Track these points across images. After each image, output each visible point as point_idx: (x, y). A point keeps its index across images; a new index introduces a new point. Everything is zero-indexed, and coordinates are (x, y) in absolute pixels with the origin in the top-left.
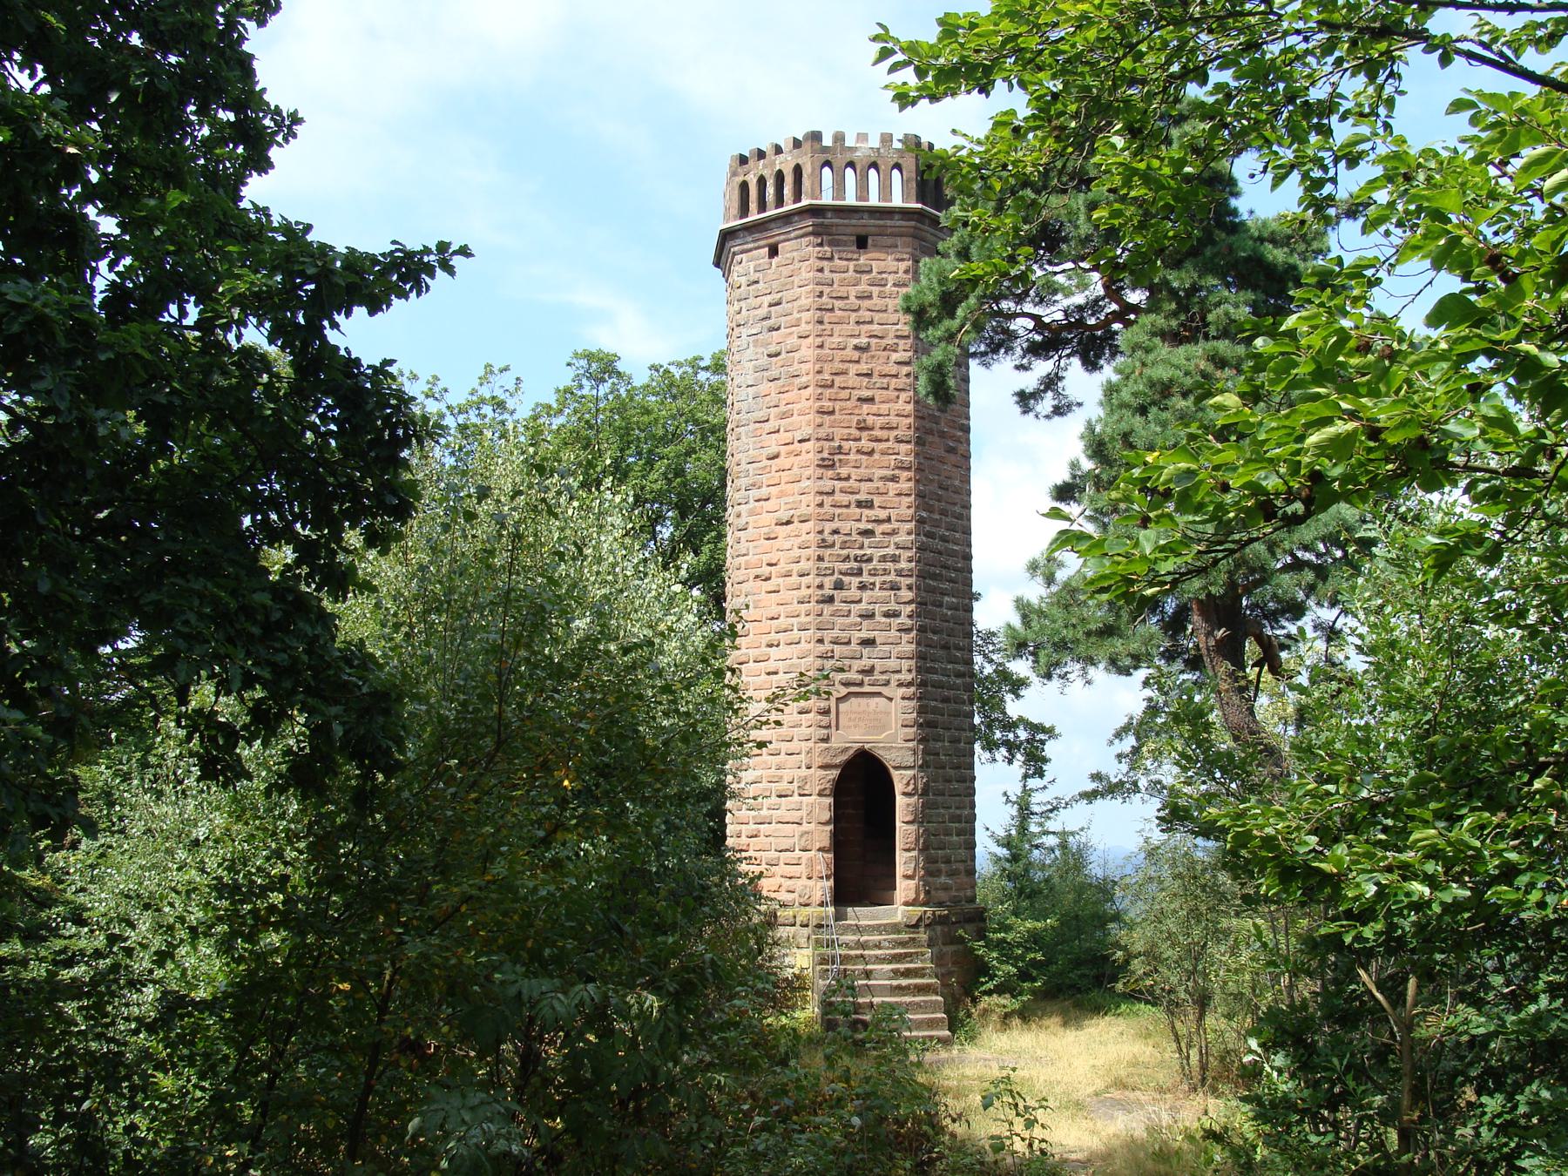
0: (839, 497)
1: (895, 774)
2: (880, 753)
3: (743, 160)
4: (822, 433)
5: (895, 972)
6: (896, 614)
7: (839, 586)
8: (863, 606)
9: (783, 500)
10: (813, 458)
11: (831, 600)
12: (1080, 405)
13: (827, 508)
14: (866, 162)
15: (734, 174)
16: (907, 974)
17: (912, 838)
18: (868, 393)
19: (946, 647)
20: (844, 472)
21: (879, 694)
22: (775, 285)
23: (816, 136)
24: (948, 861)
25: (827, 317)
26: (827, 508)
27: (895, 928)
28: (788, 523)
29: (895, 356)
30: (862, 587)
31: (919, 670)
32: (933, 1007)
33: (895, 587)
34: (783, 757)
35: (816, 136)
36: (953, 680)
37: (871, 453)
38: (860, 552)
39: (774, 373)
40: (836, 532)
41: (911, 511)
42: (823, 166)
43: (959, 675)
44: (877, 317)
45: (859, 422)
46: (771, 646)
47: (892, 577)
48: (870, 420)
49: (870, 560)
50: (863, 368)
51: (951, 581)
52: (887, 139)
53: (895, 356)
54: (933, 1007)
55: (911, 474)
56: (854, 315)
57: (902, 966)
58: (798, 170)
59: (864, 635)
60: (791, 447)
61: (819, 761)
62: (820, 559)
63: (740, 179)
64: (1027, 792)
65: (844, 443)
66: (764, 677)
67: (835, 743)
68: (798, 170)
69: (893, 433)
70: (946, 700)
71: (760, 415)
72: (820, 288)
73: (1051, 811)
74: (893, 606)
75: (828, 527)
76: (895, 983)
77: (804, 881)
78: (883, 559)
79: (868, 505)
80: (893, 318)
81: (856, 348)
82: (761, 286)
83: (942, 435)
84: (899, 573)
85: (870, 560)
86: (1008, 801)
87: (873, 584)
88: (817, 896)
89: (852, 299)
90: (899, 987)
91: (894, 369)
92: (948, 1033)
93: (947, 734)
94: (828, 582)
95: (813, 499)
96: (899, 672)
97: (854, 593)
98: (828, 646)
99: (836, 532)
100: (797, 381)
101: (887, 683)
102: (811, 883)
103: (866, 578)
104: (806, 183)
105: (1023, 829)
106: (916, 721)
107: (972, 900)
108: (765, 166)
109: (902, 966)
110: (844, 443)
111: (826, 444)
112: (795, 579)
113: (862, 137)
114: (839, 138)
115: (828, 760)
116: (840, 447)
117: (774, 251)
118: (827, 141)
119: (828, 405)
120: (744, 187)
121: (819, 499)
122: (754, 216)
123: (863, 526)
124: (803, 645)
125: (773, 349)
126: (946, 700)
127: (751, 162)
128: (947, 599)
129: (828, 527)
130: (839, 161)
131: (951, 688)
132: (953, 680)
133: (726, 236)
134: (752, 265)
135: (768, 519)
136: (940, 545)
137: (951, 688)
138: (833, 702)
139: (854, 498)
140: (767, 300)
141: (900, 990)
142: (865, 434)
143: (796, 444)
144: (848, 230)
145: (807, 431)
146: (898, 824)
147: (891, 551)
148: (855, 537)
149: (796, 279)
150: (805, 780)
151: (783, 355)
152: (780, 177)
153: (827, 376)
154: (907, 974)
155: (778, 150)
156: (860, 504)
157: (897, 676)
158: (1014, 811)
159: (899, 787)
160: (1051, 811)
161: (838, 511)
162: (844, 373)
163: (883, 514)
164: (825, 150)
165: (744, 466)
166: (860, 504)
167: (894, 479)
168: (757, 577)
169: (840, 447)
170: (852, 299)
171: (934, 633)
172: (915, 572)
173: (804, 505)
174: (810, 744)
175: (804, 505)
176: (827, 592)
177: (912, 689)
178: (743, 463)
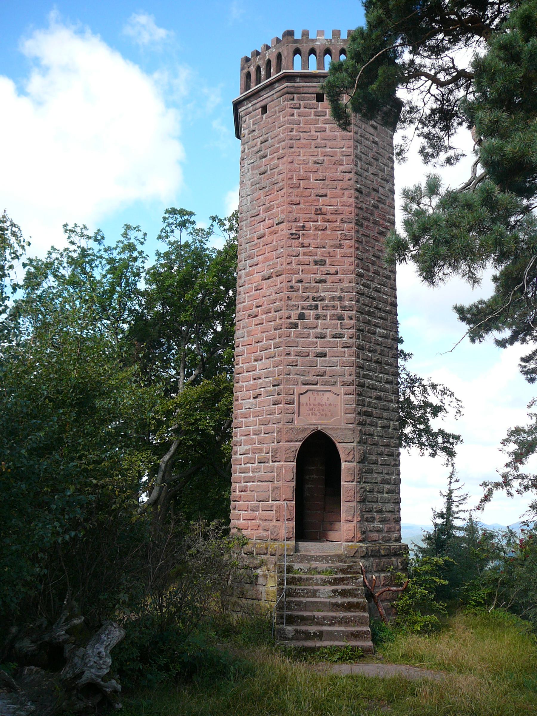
0: (301, 258)
1: (339, 446)
2: (329, 433)
3: (247, 60)
4: (292, 217)
5: (335, 591)
6: (341, 336)
7: (302, 317)
8: (319, 330)
9: (266, 264)
10: (286, 232)
11: (296, 326)
12: (464, 155)
13: (294, 266)
14: (323, 49)
15: (242, 69)
16: (343, 593)
17: (352, 493)
18: (323, 192)
19: (377, 362)
20: (306, 242)
21: (329, 391)
22: (264, 130)
23: (290, 33)
24: (380, 511)
25: (295, 143)
26: (294, 266)
27: (339, 558)
28: (269, 278)
29: (341, 168)
30: (318, 317)
31: (358, 375)
32: (360, 622)
33: (340, 318)
34: (263, 435)
35: (290, 33)
36: (383, 385)
37: (325, 229)
38: (316, 295)
39: (263, 184)
40: (300, 281)
41: (353, 267)
42: (295, 54)
43: (391, 382)
44: (329, 143)
45: (316, 210)
46: (256, 360)
47: (339, 311)
48: (325, 208)
49: (323, 300)
50: (320, 175)
51: (381, 318)
52: (336, 34)
53: (341, 168)
54: (360, 622)
55: (352, 242)
56: (314, 142)
57: (340, 588)
58: (279, 56)
59: (319, 350)
60: (272, 229)
61: (285, 437)
62: (289, 299)
63: (246, 71)
64: (451, 491)
65: (306, 224)
66: (252, 382)
67: (298, 424)
68: (279, 56)
69: (339, 217)
70: (379, 398)
71: (254, 212)
72: (291, 126)
73: (464, 499)
74: (339, 330)
75: (295, 278)
76: (333, 600)
77: (274, 523)
78: (333, 299)
79: (323, 263)
80: (341, 143)
81: (316, 163)
82: (256, 133)
83: (375, 223)
84: (344, 308)
85: (323, 300)
86: (441, 495)
87: (326, 316)
88: (283, 533)
89: (313, 133)
90: (336, 605)
91: (340, 175)
92: (370, 643)
93: (379, 422)
94: (294, 314)
95: (284, 260)
96: (343, 375)
97: (311, 321)
98: (292, 358)
99: (300, 281)
100: (276, 186)
101: (334, 384)
102: (279, 524)
103: (320, 311)
104: (284, 62)
105: (449, 508)
106: (354, 410)
107: (399, 539)
108: (260, 59)
109: (340, 588)
110: (306, 224)
111: (294, 224)
112: (273, 314)
113: (320, 33)
114: (305, 34)
115: (292, 437)
116: (304, 226)
117: (264, 109)
118: (298, 36)
119: (296, 199)
120: (248, 75)
121: (289, 260)
122: (254, 88)
123: (319, 277)
124: (277, 358)
125: (262, 169)
126: (379, 398)
127: (252, 60)
128: (378, 330)
129: (295, 278)
130: (305, 49)
131: (382, 390)
132: (383, 385)
133: (237, 105)
134: (251, 121)
135: (257, 277)
136: (374, 294)
137: (382, 390)
138: (296, 397)
139: (311, 259)
140: (259, 140)
141: (337, 606)
142: (320, 217)
143: (275, 226)
144: (311, 90)
145: (281, 217)
146: (343, 483)
147: (338, 294)
148: (313, 284)
149: (277, 123)
150: (275, 451)
151: (269, 172)
152: (269, 62)
153: (295, 181)
154: (343, 593)
155: (267, 48)
156: (316, 263)
157: (343, 379)
158: (445, 500)
159: (343, 457)
160: (464, 499)
161: (301, 268)
162: (308, 179)
163: (332, 270)
164: (296, 41)
165: (244, 246)
166: (316, 263)
167: (340, 246)
168: (249, 316)
169: (304, 226)
170: (313, 133)
171: (370, 351)
172: (355, 308)
173: (279, 264)
174: (280, 425)
175: (279, 264)
176: (293, 320)
177: (352, 387)
178: (243, 244)
